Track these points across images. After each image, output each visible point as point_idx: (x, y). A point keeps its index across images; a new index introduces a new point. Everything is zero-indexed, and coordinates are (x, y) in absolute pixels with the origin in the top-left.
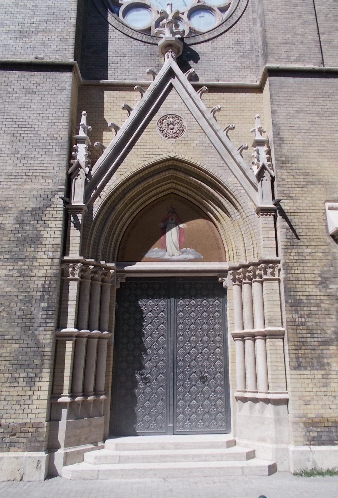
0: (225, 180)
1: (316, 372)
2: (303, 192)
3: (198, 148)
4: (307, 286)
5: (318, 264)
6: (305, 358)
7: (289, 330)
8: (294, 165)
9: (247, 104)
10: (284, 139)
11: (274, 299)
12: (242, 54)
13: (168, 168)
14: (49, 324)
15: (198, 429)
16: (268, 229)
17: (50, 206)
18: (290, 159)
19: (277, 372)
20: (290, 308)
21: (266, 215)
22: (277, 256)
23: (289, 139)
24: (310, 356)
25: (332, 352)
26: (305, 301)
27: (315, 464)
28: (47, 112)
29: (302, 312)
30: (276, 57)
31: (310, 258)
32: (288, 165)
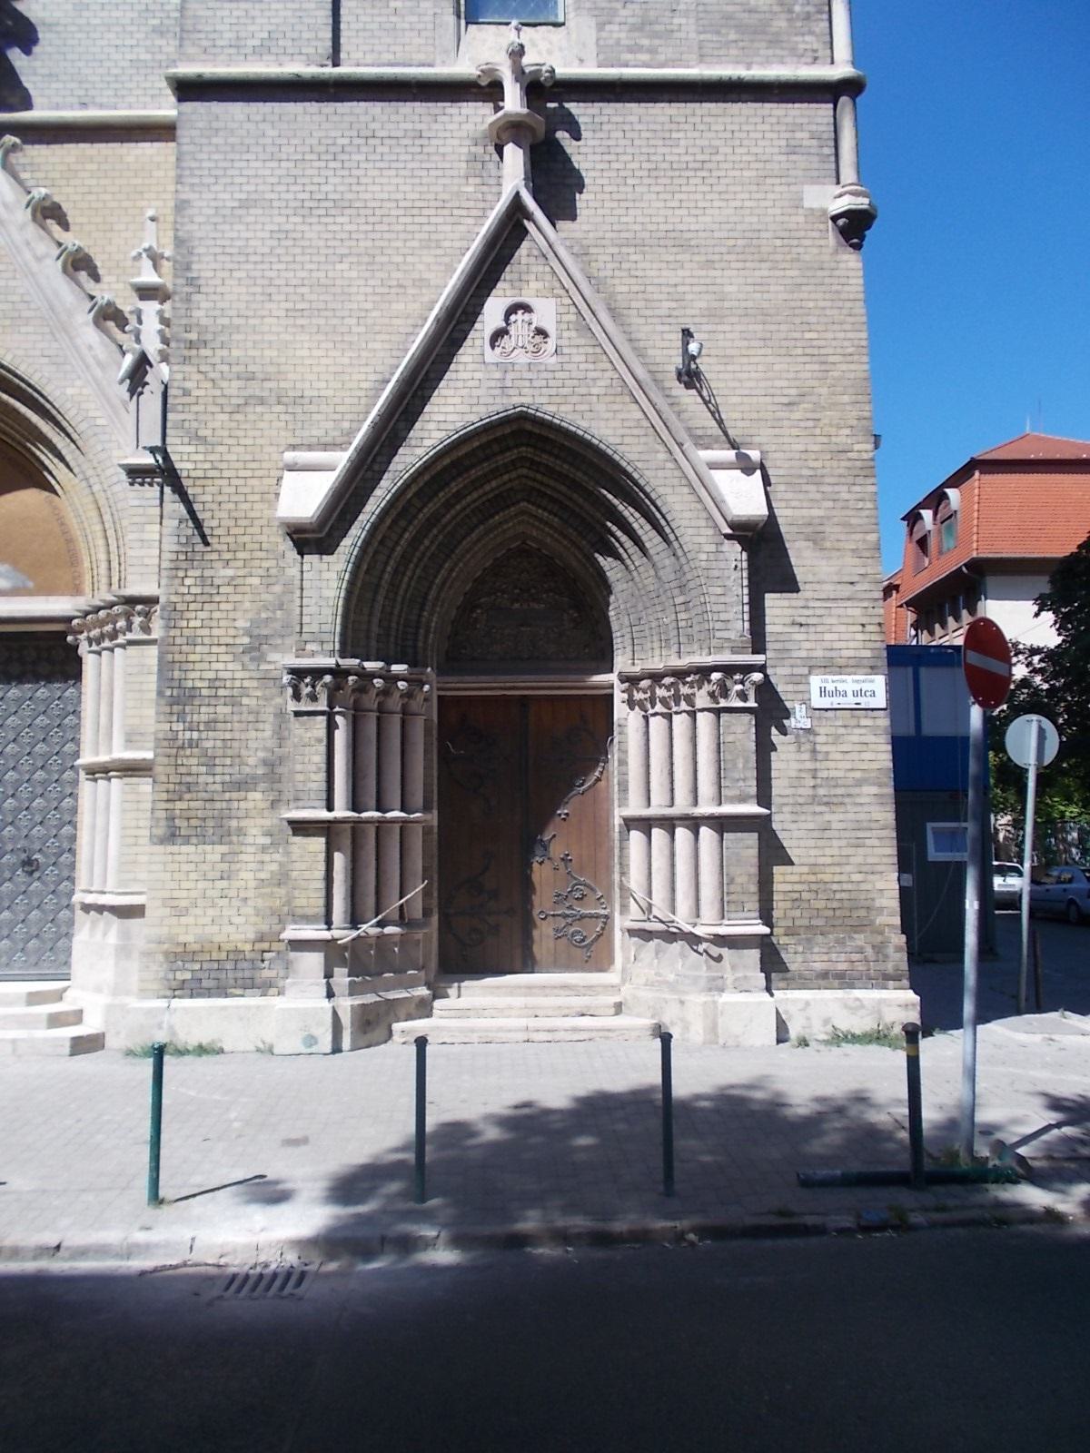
1: (208, 848)
8: (219, 353)
9: (155, 173)
10: (202, 282)
11: (145, 687)
12: (156, 22)
16: (143, 519)
18: (209, 337)
19: (135, 849)
20: (167, 709)
21: (142, 484)
24: (200, 814)
25: (250, 805)
26: (205, 692)
27: (174, 1034)
29: (195, 717)
30: (205, 43)
31: (230, 589)
32: (203, 352)
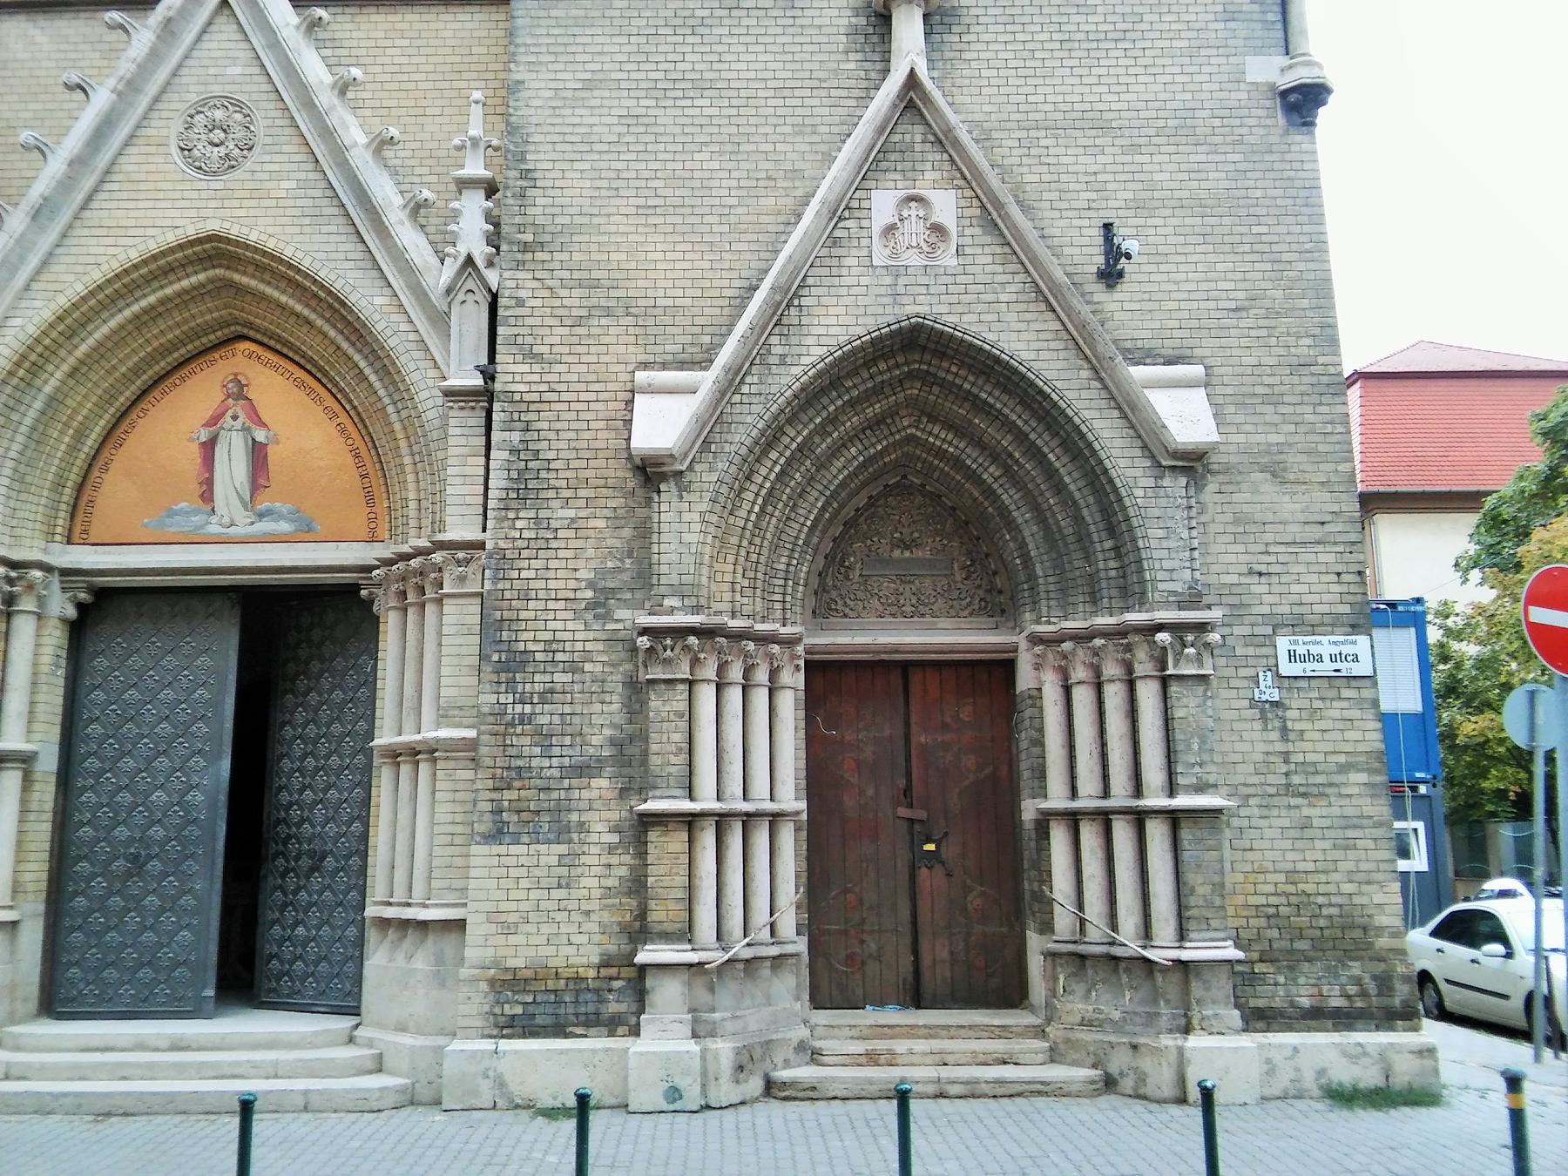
0: (364, 303)
1: (543, 848)
4: (551, 615)
5: (591, 552)
10: (538, 175)
15: (304, 997)
26: (539, 656)
31: (571, 533)
32: (539, 256)
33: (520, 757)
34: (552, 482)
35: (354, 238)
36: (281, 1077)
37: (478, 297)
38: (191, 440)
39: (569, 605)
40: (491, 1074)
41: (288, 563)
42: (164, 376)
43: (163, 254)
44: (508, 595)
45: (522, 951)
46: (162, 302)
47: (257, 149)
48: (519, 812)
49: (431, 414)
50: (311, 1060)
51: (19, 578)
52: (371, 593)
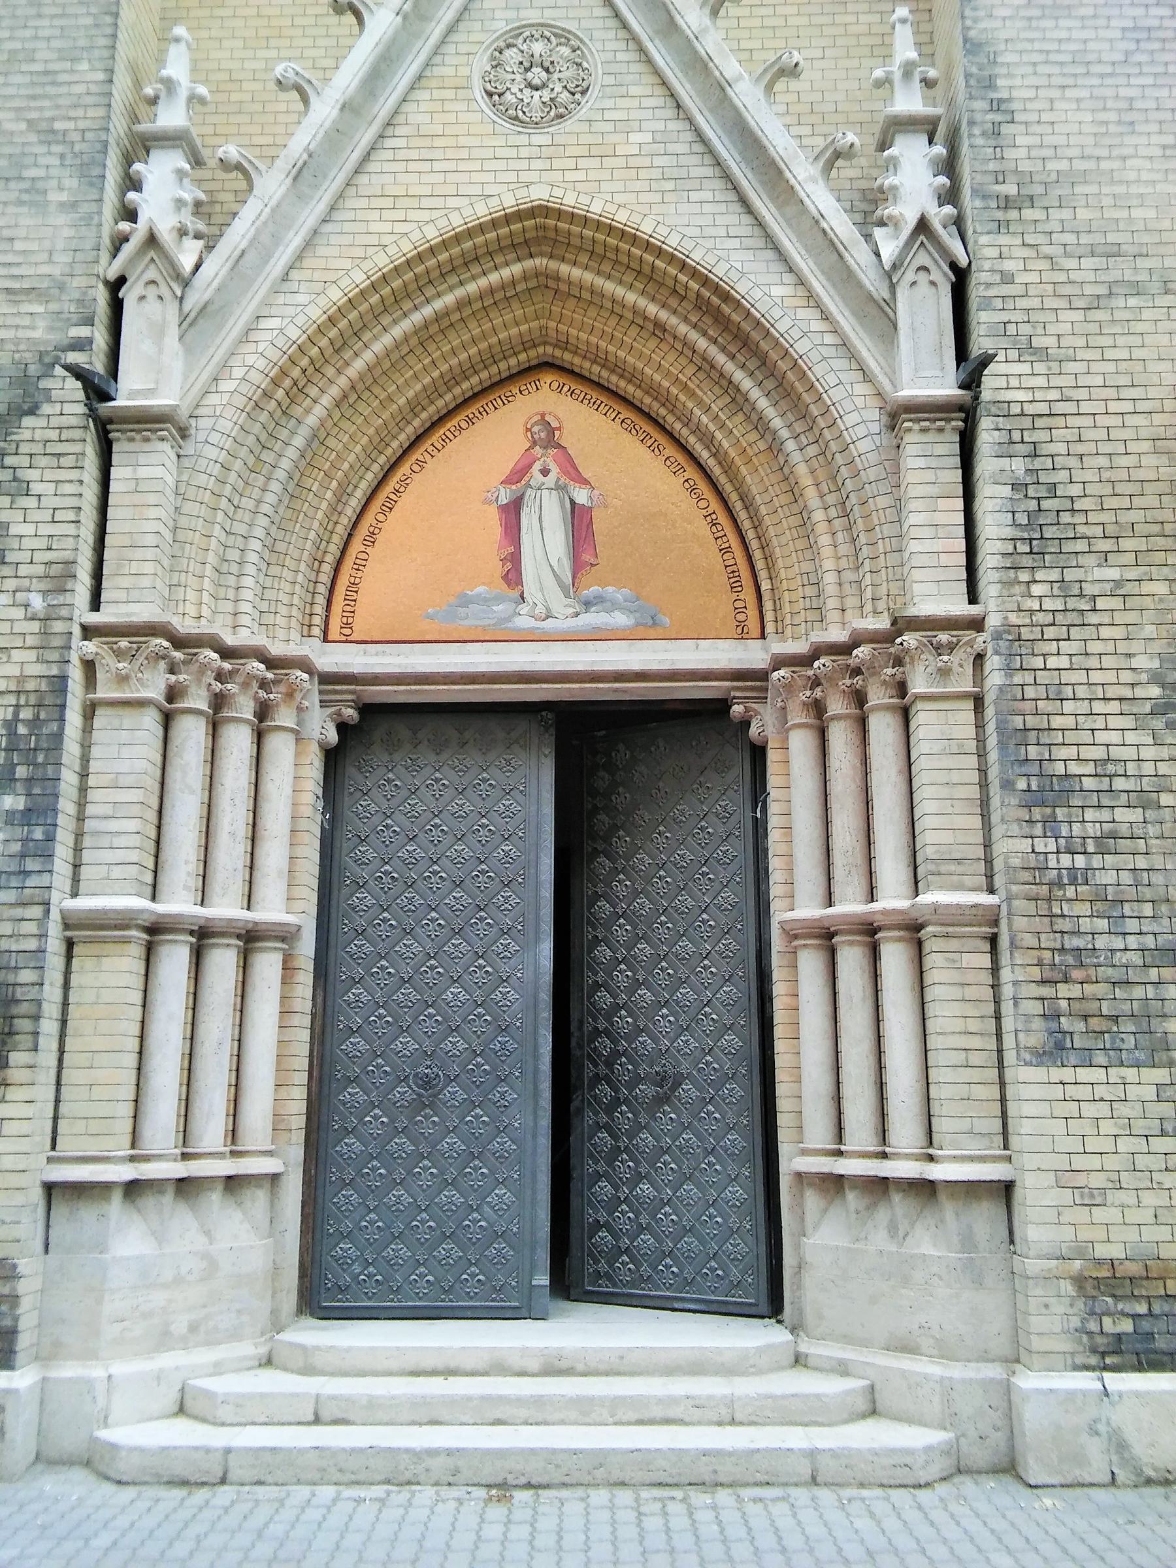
0: (757, 294)
1: (1130, 1073)
2: (1093, 327)
3: (647, 162)
4: (1100, 723)
5: (1150, 631)
6: (1086, 1017)
7: (1016, 903)
10: (1015, 106)
13: (522, 246)
14: (34, 876)
15: (658, 1288)
17: (32, 412)
18: (1038, 189)
22: (973, 599)
23: (1036, 105)
26: (1088, 783)
28: (28, 33)
31: (1116, 603)
32: (1028, 214)
33: (1078, 933)
34: (1082, 530)
35: (737, 208)
36: (741, 1424)
37: (936, 275)
38: (487, 502)
39: (1126, 707)
40: (1102, 1428)
41: (636, 667)
42: (445, 415)
43: (469, 233)
44: (1030, 692)
45: (1116, 1234)
46: (460, 305)
47: (593, 93)
48: (1086, 1017)
49: (864, 446)
50: (784, 1397)
51: (276, 682)
52: (747, 710)
